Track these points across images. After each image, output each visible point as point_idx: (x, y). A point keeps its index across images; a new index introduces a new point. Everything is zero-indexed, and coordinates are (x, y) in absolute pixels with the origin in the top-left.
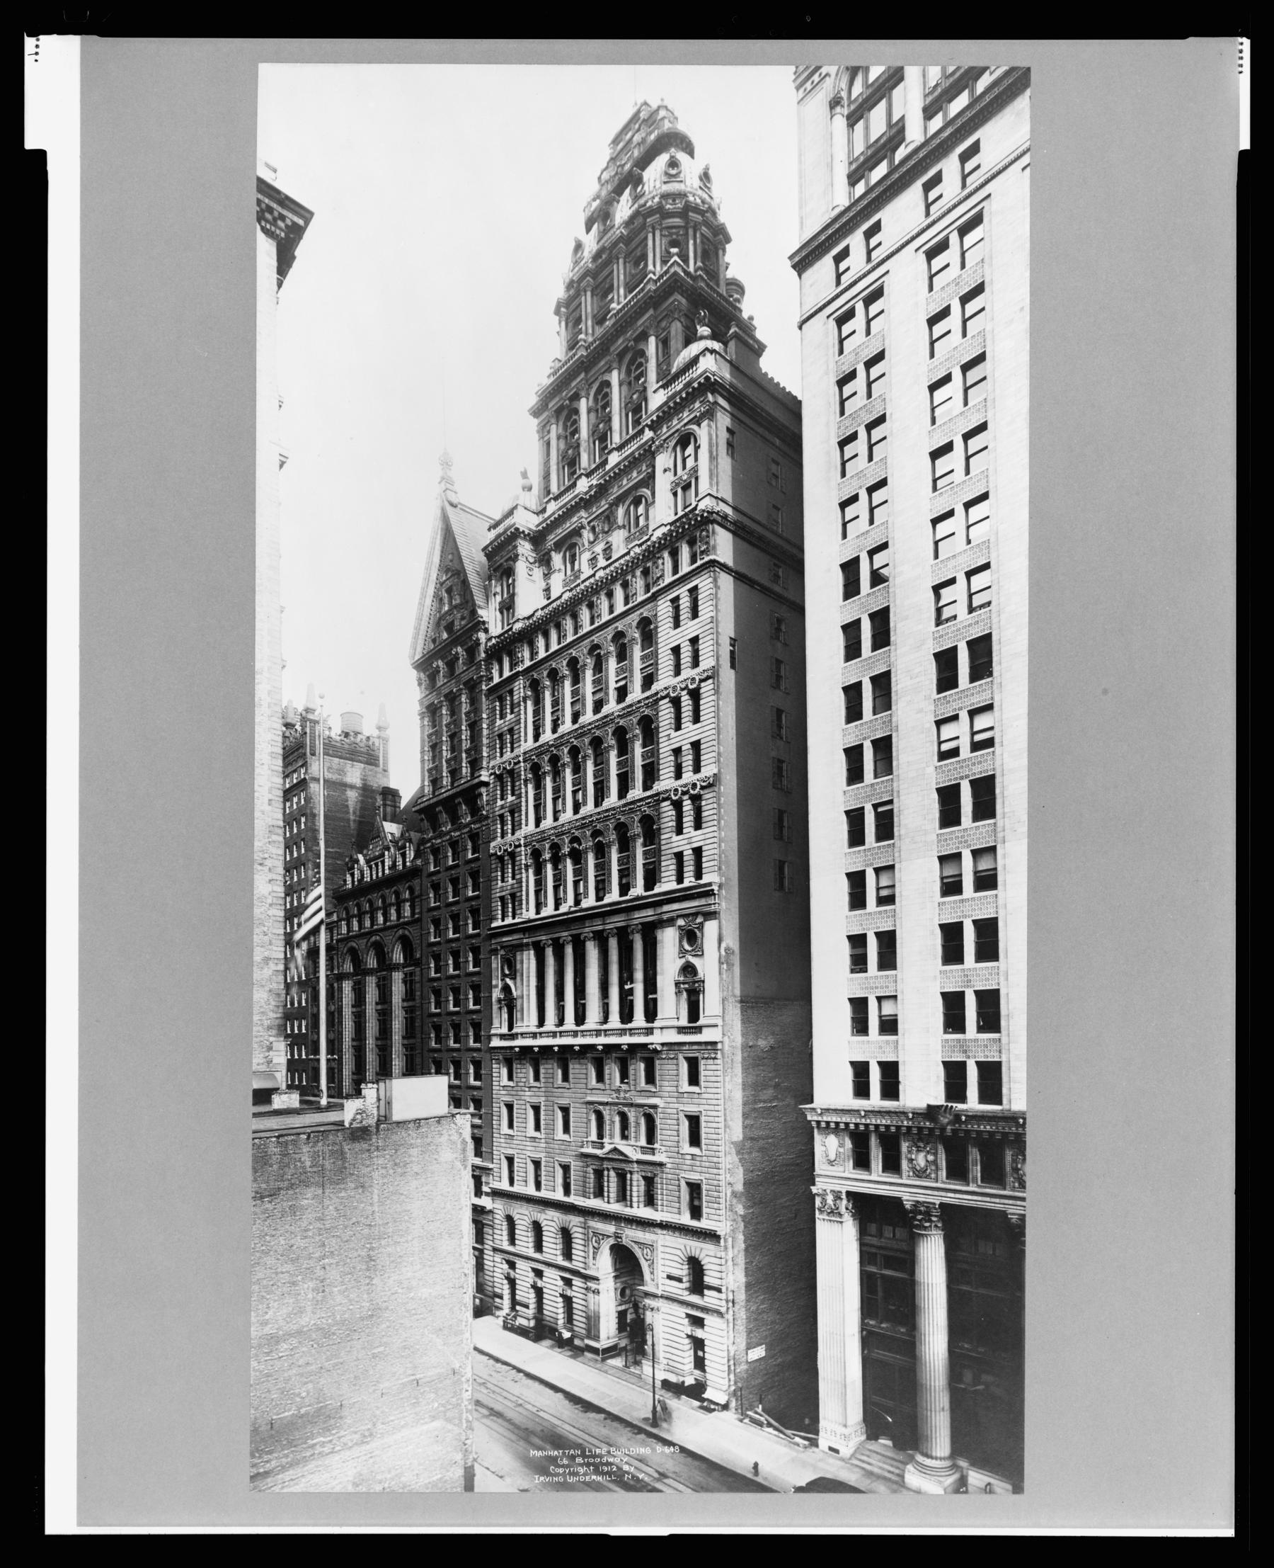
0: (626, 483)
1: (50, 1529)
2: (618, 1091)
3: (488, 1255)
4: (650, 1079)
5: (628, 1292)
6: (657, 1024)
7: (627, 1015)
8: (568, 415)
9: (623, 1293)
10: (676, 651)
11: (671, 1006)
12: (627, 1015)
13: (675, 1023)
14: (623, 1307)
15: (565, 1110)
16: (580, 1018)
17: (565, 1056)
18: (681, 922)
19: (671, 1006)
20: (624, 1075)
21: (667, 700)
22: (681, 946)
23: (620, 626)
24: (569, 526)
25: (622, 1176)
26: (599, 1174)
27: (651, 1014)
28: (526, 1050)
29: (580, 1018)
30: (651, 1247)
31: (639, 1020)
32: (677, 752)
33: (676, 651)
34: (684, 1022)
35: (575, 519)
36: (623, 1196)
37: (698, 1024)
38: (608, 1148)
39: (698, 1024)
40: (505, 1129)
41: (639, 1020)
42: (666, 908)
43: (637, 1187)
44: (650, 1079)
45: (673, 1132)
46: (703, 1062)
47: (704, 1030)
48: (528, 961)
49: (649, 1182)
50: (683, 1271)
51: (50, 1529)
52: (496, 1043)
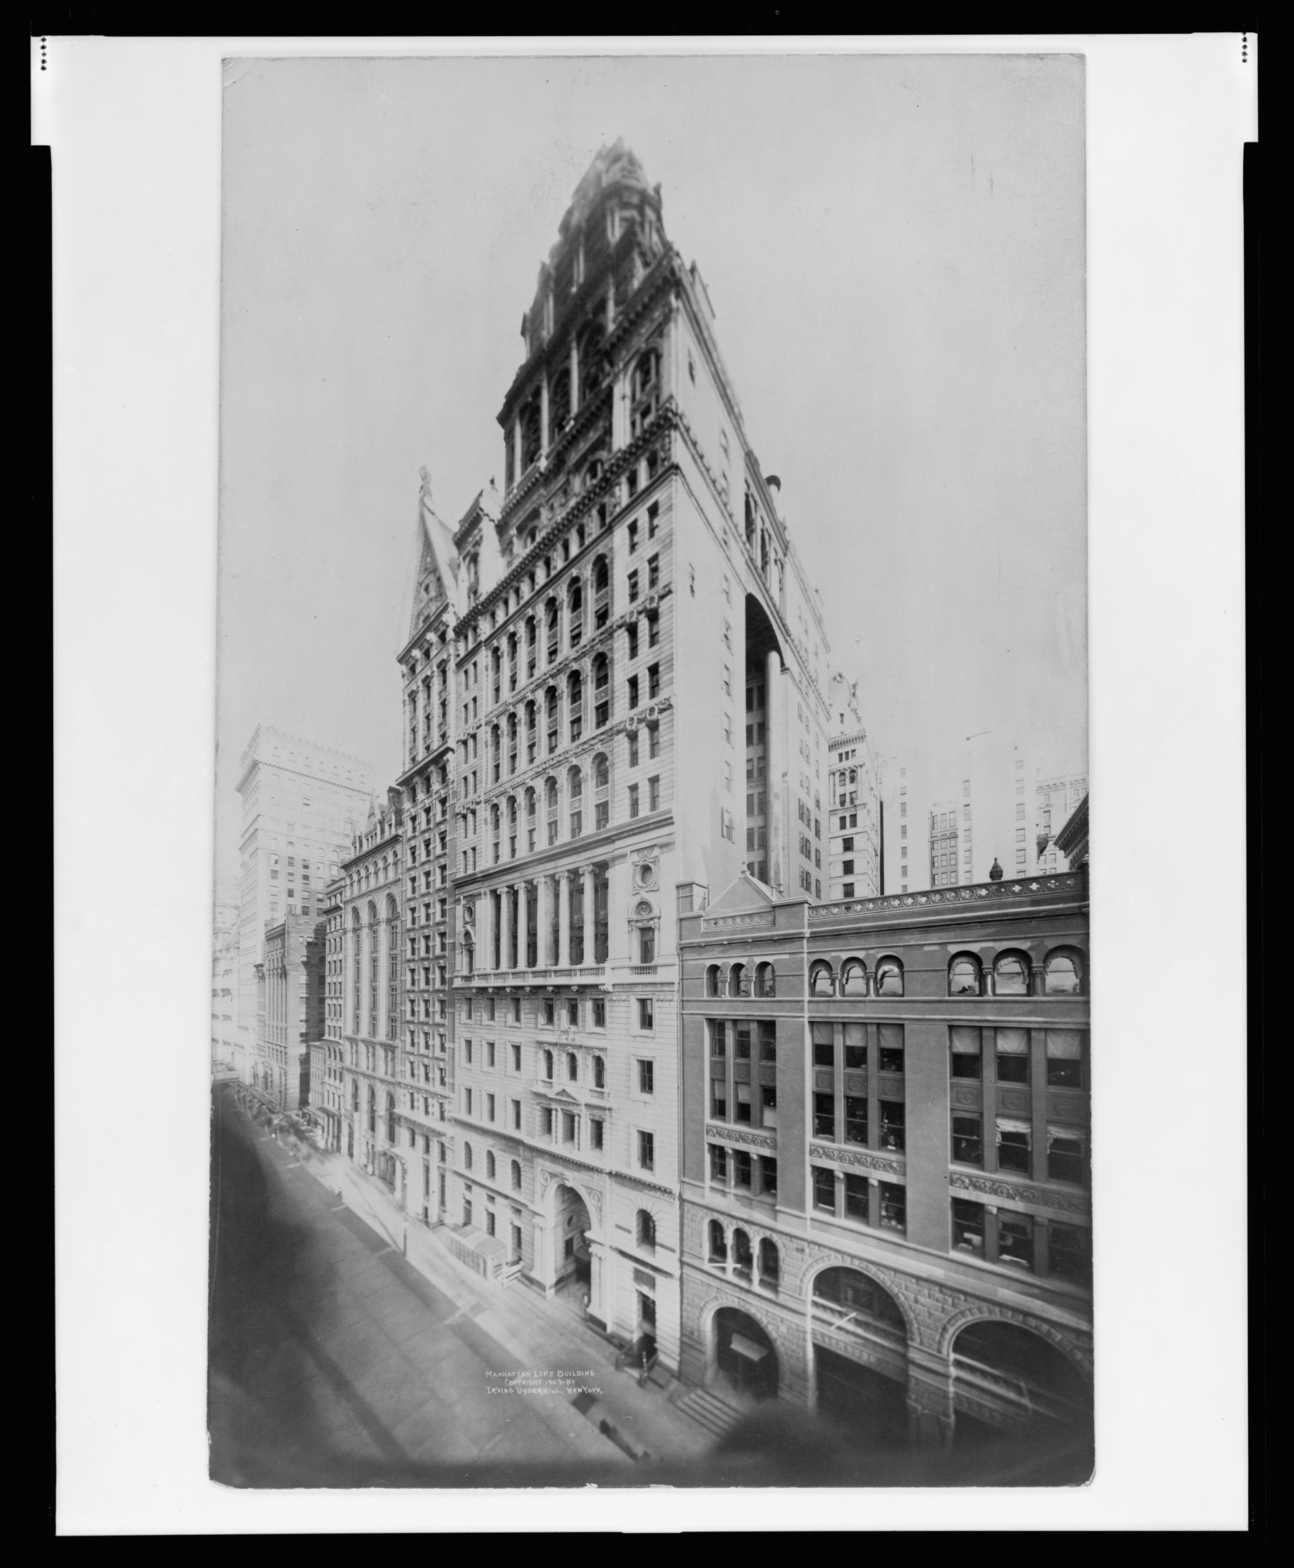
0: (583, 446)
1: (82, 1510)
2: (566, 1032)
3: (449, 1178)
4: (600, 1020)
5: (575, 1219)
6: (608, 965)
7: (577, 956)
8: (531, 414)
9: (570, 1221)
10: (633, 682)
11: (623, 944)
12: (577, 956)
13: (627, 963)
14: (570, 1236)
15: (517, 1049)
16: (532, 961)
17: (516, 996)
18: (635, 857)
19: (623, 944)
20: (574, 1020)
21: (623, 734)
22: (634, 881)
23: (574, 572)
24: (528, 507)
25: (571, 1118)
26: (548, 1112)
27: (602, 955)
28: (483, 990)
29: (532, 961)
30: (600, 1196)
31: (589, 959)
32: (634, 788)
33: (633, 682)
34: (637, 962)
35: (535, 498)
36: (570, 1134)
37: (653, 964)
38: (557, 1088)
39: (653, 964)
40: (464, 1063)
41: (589, 959)
42: (619, 844)
43: (585, 1130)
44: (600, 1020)
45: (622, 1074)
46: (656, 1004)
47: (659, 969)
48: (484, 907)
49: (598, 1126)
50: (633, 1223)
51: (82, 1510)
52: (458, 983)
